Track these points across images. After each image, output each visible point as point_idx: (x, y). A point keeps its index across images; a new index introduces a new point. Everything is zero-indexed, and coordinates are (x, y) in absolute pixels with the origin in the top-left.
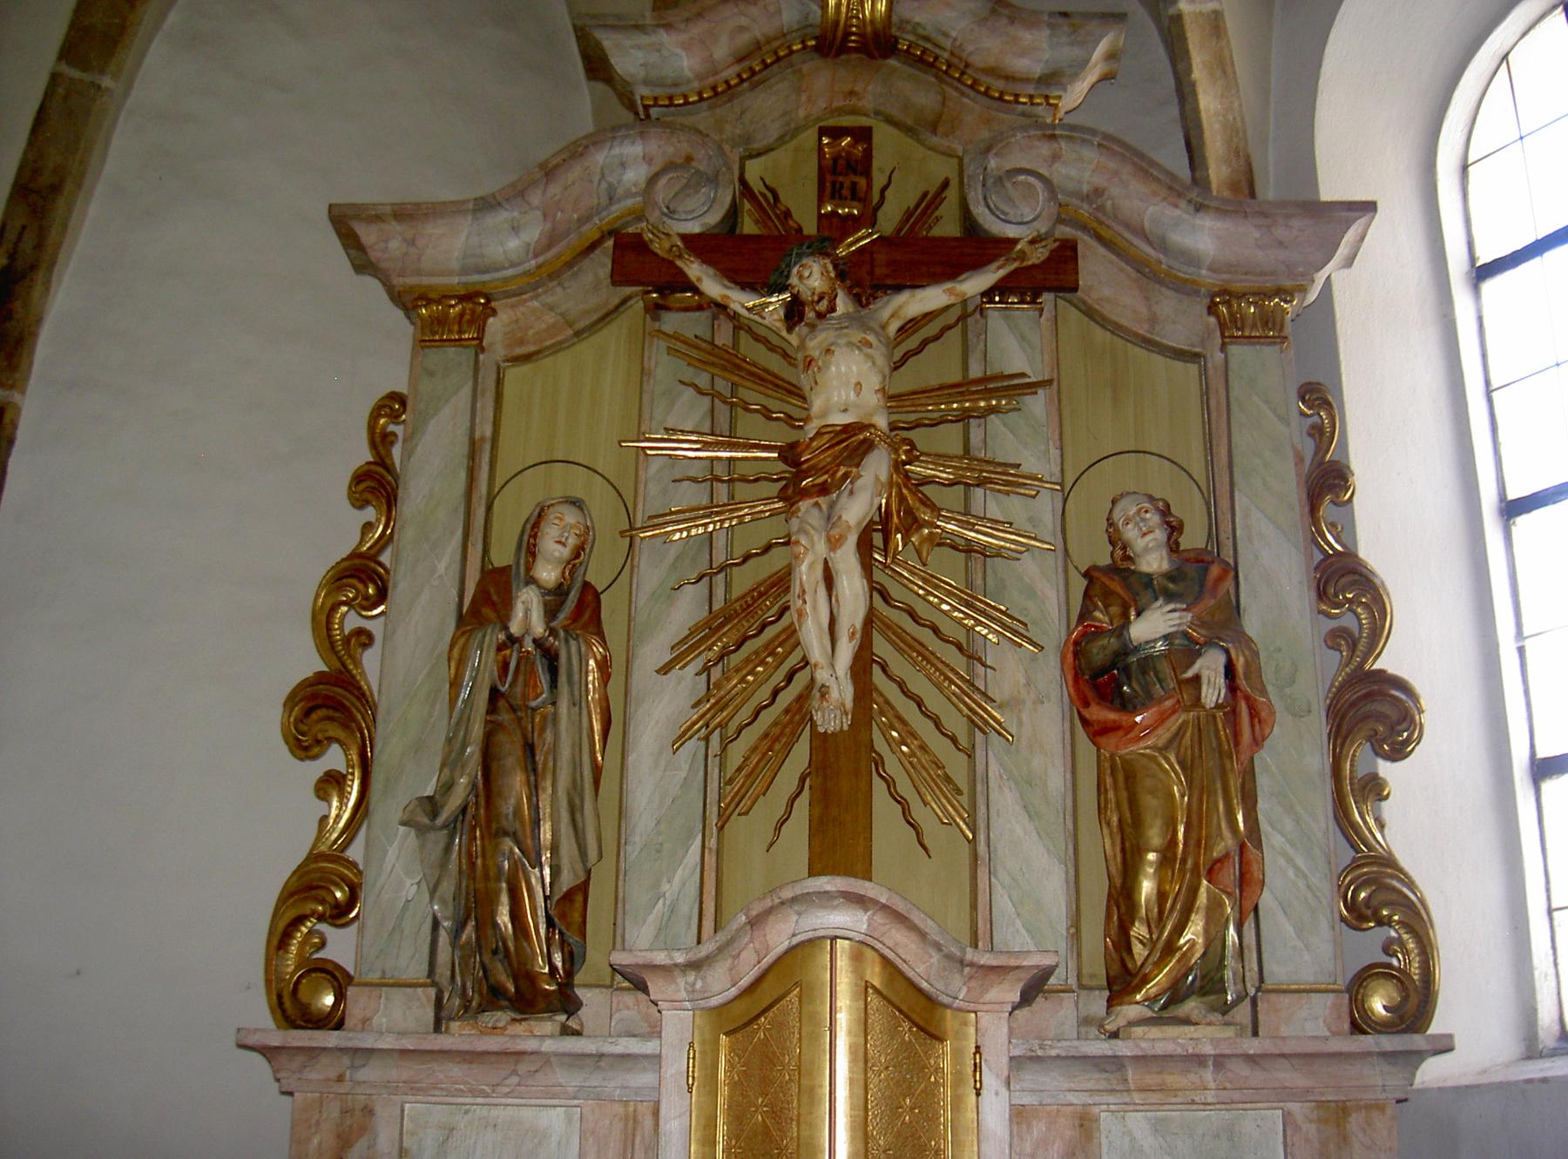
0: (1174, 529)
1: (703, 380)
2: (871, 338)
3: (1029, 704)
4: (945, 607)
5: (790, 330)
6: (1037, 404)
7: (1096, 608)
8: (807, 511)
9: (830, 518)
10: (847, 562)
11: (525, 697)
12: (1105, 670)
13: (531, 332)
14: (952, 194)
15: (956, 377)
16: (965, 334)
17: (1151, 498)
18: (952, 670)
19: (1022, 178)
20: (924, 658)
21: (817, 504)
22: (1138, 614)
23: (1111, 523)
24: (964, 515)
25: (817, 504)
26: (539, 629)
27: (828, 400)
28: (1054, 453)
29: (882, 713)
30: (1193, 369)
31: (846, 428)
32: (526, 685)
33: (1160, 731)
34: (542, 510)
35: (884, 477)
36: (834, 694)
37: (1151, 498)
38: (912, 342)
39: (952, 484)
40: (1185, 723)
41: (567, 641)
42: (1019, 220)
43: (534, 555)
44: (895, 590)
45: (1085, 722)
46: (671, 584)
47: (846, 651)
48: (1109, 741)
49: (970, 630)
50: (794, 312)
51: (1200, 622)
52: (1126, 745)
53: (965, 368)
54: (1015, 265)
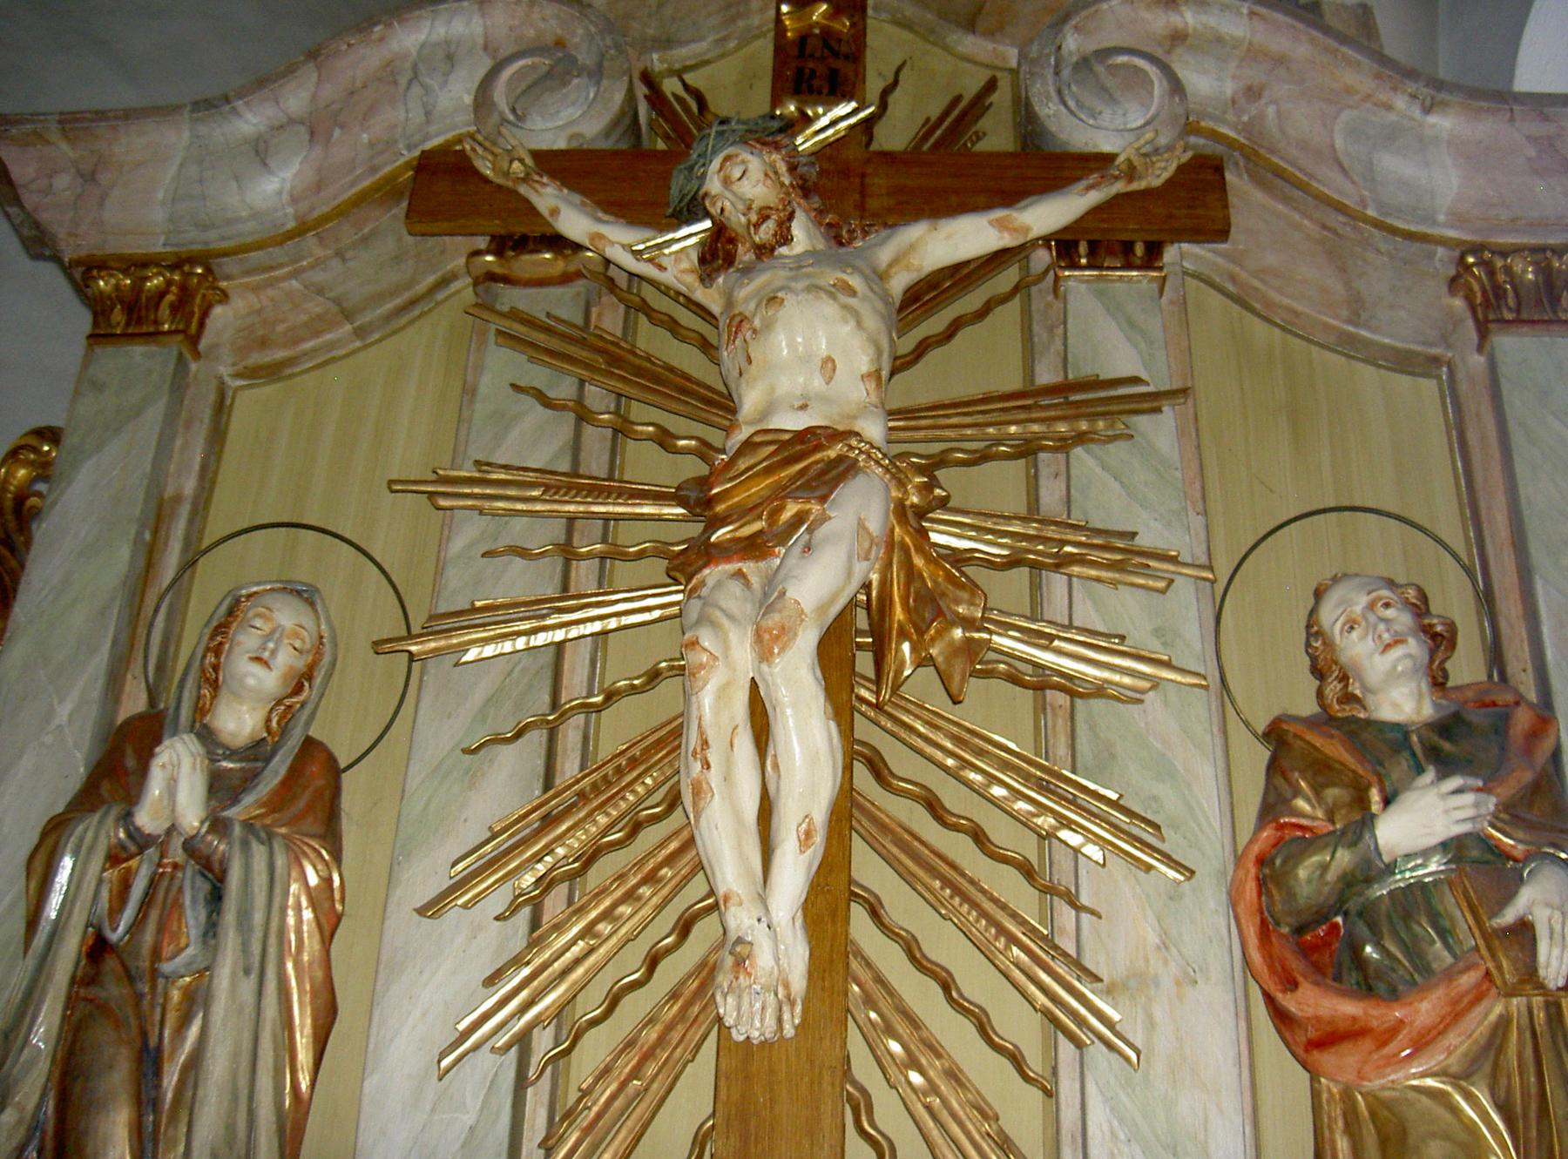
0: (1440, 641)
1: (564, 389)
2: (855, 281)
3: (1167, 983)
4: (998, 791)
5: (706, 278)
6: (1160, 431)
7: (1297, 792)
8: (719, 584)
9: (770, 598)
10: (797, 688)
11: (156, 954)
12: (1322, 915)
13: (281, 328)
14: (1001, 98)
15: (1014, 383)
16: (1026, 313)
17: (1391, 584)
18: (1014, 915)
19: (1122, 59)
20: (957, 891)
21: (739, 574)
22: (1387, 801)
23: (1313, 630)
24: (1033, 619)
25: (739, 574)
26: (191, 813)
27: (773, 389)
28: (1197, 522)
29: (869, 1002)
30: (1428, 386)
31: (801, 436)
32: (161, 929)
33: (1452, 1038)
34: (238, 601)
35: (875, 525)
36: (764, 959)
37: (1391, 584)
38: (935, 324)
39: (1012, 563)
40: (1504, 1022)
41: (245, 845)
42: (1116, 127)
43: (215, 686)
44: (899, 760)
45: (1281, 1017)
46: (465, 745)
47: (793, 871)
48: (1342, 1064)
49: (1047, 837)
50: (718, 253)
51: (1510, 815)
52: (1380, 1069)
53: (1029, 372)
54: (1119, 187)
